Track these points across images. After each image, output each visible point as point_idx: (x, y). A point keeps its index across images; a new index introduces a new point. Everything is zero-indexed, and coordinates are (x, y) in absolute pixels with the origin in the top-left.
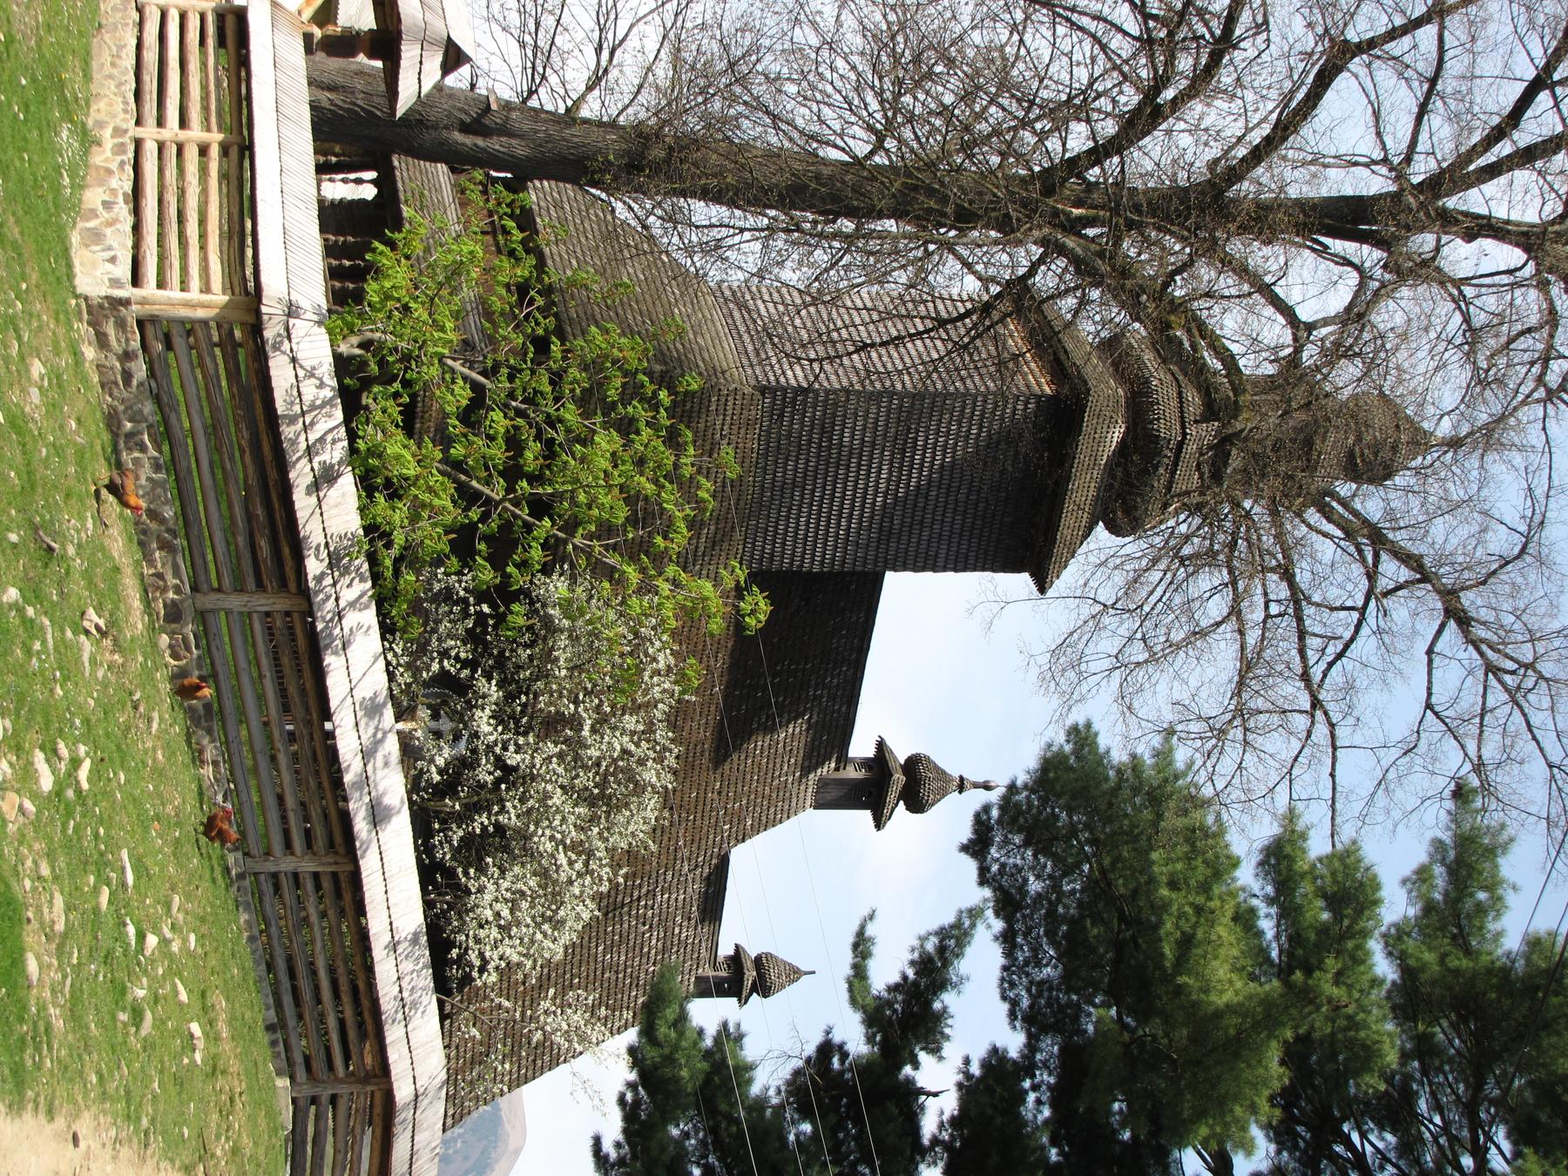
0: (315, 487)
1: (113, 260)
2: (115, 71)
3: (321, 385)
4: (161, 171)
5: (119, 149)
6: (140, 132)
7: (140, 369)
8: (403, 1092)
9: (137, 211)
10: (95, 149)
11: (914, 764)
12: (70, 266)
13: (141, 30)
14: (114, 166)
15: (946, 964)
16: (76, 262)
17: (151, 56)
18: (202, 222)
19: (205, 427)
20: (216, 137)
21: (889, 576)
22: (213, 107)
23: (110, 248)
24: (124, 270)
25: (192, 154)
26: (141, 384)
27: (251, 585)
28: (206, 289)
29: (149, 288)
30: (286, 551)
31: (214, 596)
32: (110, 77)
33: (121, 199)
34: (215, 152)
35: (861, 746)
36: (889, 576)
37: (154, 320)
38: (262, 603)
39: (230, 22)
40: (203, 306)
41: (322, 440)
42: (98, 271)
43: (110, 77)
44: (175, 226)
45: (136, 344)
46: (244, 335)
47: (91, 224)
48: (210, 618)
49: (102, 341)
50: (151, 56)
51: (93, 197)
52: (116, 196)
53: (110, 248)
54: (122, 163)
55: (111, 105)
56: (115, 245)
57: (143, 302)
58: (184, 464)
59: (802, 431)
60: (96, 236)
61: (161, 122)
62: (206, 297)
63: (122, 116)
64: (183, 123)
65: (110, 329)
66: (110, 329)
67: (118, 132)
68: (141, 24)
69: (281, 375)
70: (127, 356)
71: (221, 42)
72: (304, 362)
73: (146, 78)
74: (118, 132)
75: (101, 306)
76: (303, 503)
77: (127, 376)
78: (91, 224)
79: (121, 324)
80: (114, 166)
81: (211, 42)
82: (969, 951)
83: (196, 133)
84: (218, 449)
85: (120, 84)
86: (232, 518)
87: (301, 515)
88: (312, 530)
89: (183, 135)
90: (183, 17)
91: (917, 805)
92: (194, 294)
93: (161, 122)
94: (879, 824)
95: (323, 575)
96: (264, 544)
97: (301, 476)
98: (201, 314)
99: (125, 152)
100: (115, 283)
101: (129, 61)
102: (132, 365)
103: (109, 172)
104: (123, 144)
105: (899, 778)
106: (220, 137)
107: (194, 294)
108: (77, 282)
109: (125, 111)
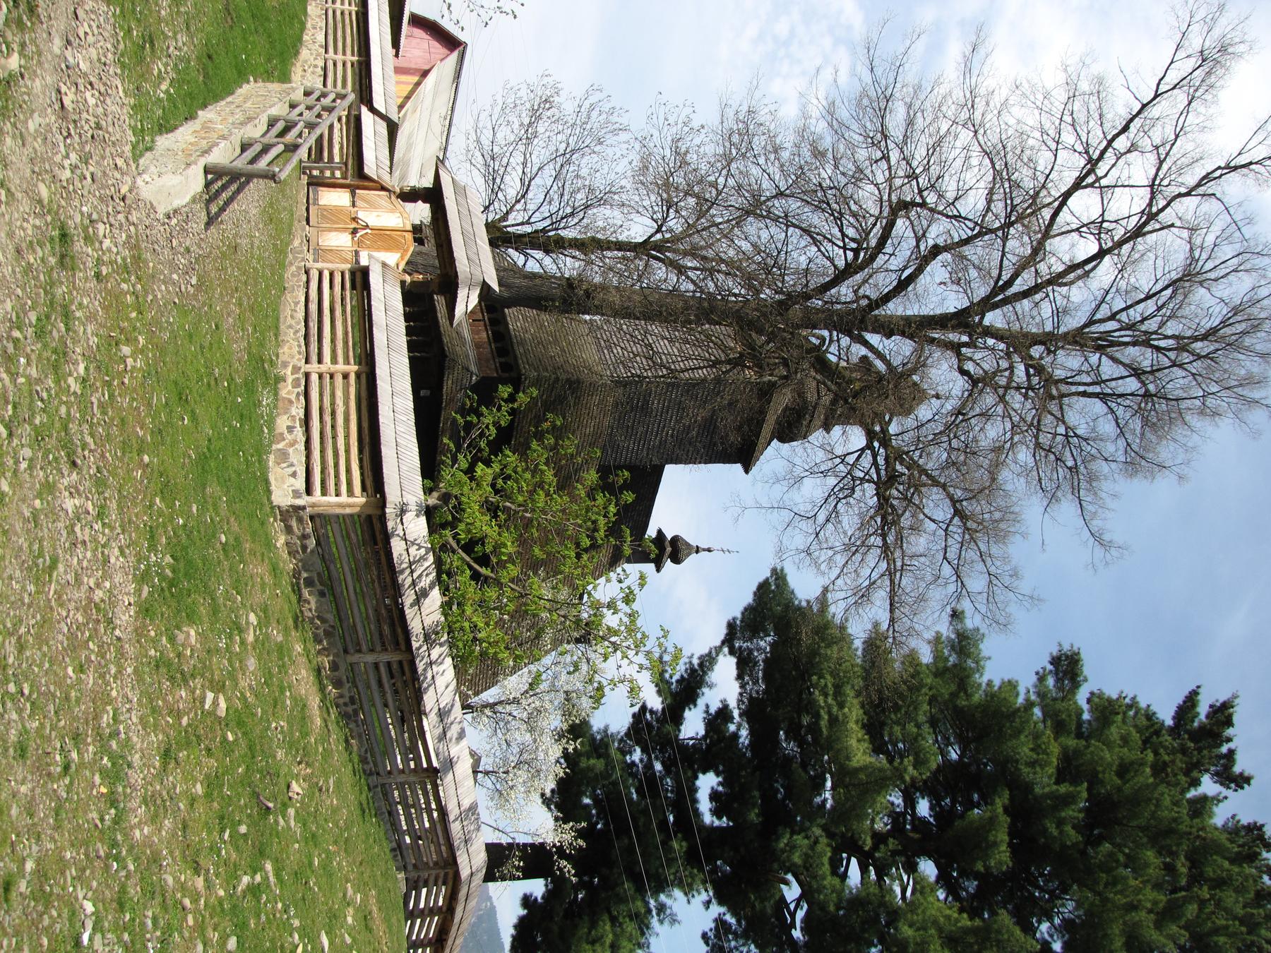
0: (417, 602)
1: (294, 475)
2: (293, 322)
3: (420, 547)
4: (321, 395)
5: (296, 383)
6: (308, 368)
7: (312, 543)
8: (464, 873)
9: (307, 345)
10: (281, 385)
11: (675, 540)
12: (267, 482)
13: (308, 288)
14: (293, 397)
15: (705, 673)
16: (272, 478)
17: (313, 307)
18: (347, 437)
19: (351, 570)
20: (353, 368)
21: (671, 471)
22: (351, 344)
23: (292, 465)
24: (300, 484)
25: (339, 380)
26: (312, 551)
27: (379, 648)
28: (350, 493)
29: (317, 496)
30: (399, 630)
31: (358, 656)
32: (290, 327)
33: (298, 424)
34: (352, 377)
35: (651, 532)
36: (669, 468)
37: (319, 515)
38: (384, 658)
39: (359, 275)
40: (350, 506)
41: (420, 576)
42: (285, 488)
43: (290, 327)
44: (330, 441)
45: (309, 530)
46: (373, 528)
47: (280, 446)
48: (356, 667)
49: (289, 529)
50: (313, 307)
51: (282, 423)
52: (294, 421)
53: (292, 465)
54: (298, 394)
55: (290, 348)
56: (295, 462)
57: (313, 505)
58: (338, 590)
59: (634, 397)
60: (283, 456)
61: (320, 361)
62: (351, 500)
63: (297, 356)
64: (334, 360)
65: (294, 523)
66: (294, 523)
67: (296, 369)
68: (308, 282)
69: (397, 546)
70: (304, 537)
71: (353, 287)
72: (411, 533)
73: (311, 324)
74: (296, 369)
75: (288, 511)
76: (409, 613)
77: (304, 548)
78: (280, 446)
79: (300, 520)
80: (293, 397)
81: (348, 285)
82: (716, 668)
83: (341, 367)
84: (359, 581)
85: (297, 332)
86: (368, 617)
87: (409, 617)
88: (415, 626)
89: (333, 368)
90: (332, 274)
91: (676, 559)
92: (344, 498)
93: (320, 361)
94: (658, 570)
95: (420, 647)
96: (386, 629)
97: (408, 598)
98: (348, 511)
99: (299, 386)
100: (296, 494)
101: (301, 315)
102: (307, 542)
103: (291, 402)
104: (298, 379)
105: (669, 549)
106: (356, 368)
107: (344, 498)
108: (273, 498)
109: (299, 353)
